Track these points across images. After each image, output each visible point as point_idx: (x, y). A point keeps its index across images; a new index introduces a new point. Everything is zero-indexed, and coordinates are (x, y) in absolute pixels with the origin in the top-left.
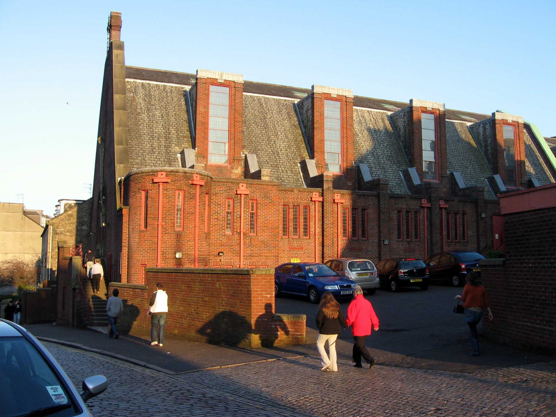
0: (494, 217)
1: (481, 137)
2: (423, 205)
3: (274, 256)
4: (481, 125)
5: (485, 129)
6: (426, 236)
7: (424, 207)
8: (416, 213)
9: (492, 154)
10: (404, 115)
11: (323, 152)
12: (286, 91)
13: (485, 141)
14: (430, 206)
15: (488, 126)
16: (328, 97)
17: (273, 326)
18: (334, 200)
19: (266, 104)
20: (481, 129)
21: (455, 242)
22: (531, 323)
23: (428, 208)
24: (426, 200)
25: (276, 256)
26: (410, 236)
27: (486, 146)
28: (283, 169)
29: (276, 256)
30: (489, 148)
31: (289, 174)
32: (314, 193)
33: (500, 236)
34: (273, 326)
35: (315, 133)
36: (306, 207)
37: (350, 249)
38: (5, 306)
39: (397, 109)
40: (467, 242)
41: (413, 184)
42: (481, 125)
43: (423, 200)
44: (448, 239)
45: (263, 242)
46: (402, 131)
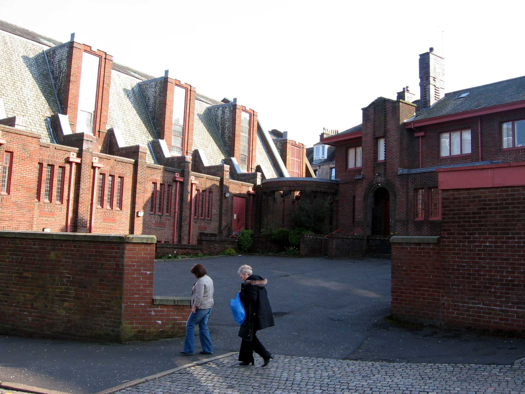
0: (234, 198)
1: (219, 120)
2: (177, 179)
3: (27, 221)
4: (221, 108)
5: (223, 112)
6: (177, 211)
7: (176, 181)
8: (169, 186)
9: (229, 137)
10: (156, 86)
11: (76, 109)
12: (33, 37)
13: (223, 124)
14: (182, 180)
15: (227, 110)
16: (89, 50)
17: (153, 313)
18: (93, 163)
19: (12, 44)
20: (220, 112)
21: (201, 219)
22: (484, 304)
23: (180, 182)
24: (178, 174)
25: (30, 222)
26: (169, 211)
27: (223, 129)
28: (31, 121)
29: (30, 222)
30: (226, 131)
31: (37, 128)
32: (72, 153)
33: (237, 217)
34: (153, 313)
35: (71, 87)
36: (63, 168)
37: (104, 219)
38: (365, 184)
39: (145, 79)
40: (211, 220)
41: (164, 156)
42: (221, 108)
43: (176, 174)
44: (195, 215)
45: (15, 203)
46: (152, 101)
